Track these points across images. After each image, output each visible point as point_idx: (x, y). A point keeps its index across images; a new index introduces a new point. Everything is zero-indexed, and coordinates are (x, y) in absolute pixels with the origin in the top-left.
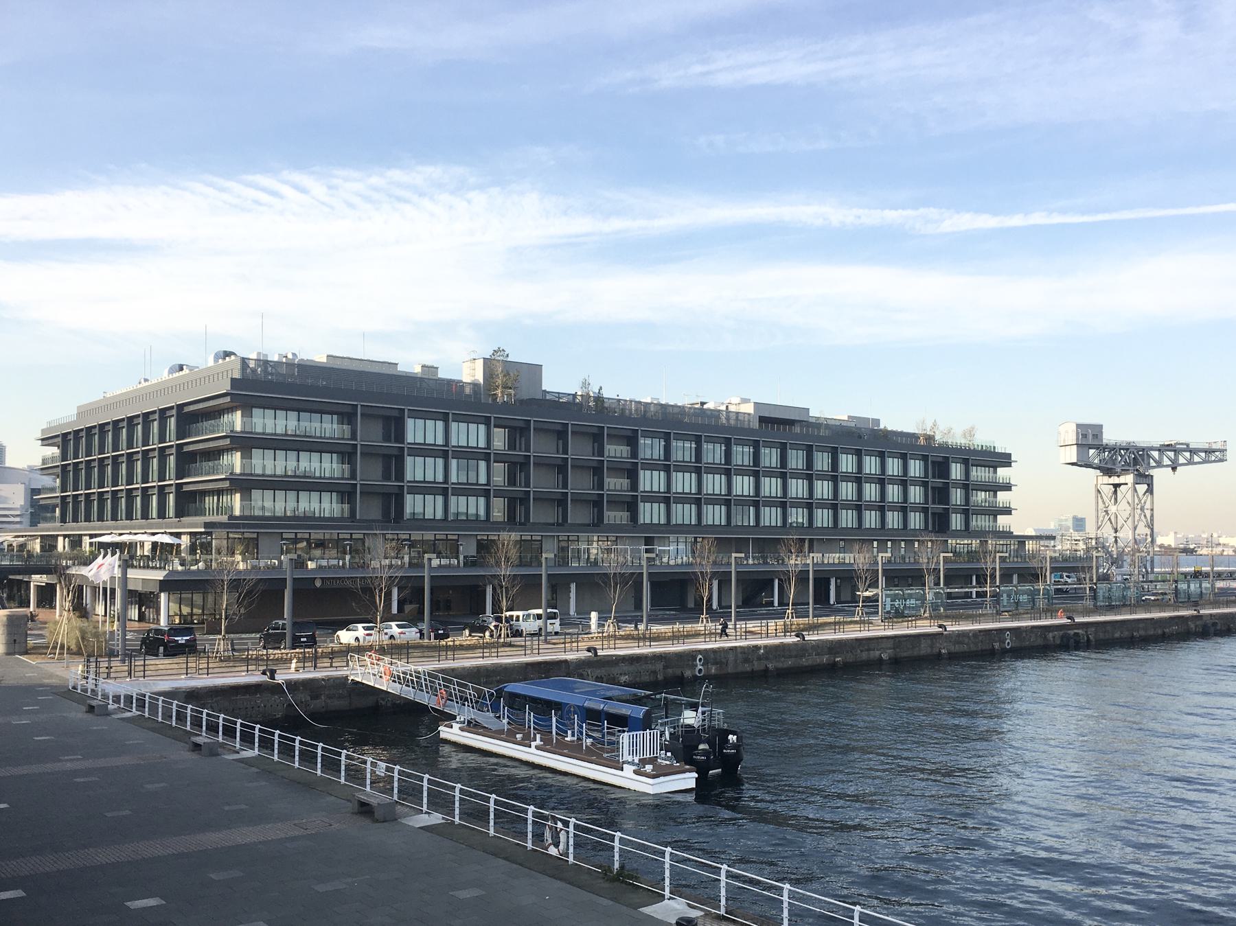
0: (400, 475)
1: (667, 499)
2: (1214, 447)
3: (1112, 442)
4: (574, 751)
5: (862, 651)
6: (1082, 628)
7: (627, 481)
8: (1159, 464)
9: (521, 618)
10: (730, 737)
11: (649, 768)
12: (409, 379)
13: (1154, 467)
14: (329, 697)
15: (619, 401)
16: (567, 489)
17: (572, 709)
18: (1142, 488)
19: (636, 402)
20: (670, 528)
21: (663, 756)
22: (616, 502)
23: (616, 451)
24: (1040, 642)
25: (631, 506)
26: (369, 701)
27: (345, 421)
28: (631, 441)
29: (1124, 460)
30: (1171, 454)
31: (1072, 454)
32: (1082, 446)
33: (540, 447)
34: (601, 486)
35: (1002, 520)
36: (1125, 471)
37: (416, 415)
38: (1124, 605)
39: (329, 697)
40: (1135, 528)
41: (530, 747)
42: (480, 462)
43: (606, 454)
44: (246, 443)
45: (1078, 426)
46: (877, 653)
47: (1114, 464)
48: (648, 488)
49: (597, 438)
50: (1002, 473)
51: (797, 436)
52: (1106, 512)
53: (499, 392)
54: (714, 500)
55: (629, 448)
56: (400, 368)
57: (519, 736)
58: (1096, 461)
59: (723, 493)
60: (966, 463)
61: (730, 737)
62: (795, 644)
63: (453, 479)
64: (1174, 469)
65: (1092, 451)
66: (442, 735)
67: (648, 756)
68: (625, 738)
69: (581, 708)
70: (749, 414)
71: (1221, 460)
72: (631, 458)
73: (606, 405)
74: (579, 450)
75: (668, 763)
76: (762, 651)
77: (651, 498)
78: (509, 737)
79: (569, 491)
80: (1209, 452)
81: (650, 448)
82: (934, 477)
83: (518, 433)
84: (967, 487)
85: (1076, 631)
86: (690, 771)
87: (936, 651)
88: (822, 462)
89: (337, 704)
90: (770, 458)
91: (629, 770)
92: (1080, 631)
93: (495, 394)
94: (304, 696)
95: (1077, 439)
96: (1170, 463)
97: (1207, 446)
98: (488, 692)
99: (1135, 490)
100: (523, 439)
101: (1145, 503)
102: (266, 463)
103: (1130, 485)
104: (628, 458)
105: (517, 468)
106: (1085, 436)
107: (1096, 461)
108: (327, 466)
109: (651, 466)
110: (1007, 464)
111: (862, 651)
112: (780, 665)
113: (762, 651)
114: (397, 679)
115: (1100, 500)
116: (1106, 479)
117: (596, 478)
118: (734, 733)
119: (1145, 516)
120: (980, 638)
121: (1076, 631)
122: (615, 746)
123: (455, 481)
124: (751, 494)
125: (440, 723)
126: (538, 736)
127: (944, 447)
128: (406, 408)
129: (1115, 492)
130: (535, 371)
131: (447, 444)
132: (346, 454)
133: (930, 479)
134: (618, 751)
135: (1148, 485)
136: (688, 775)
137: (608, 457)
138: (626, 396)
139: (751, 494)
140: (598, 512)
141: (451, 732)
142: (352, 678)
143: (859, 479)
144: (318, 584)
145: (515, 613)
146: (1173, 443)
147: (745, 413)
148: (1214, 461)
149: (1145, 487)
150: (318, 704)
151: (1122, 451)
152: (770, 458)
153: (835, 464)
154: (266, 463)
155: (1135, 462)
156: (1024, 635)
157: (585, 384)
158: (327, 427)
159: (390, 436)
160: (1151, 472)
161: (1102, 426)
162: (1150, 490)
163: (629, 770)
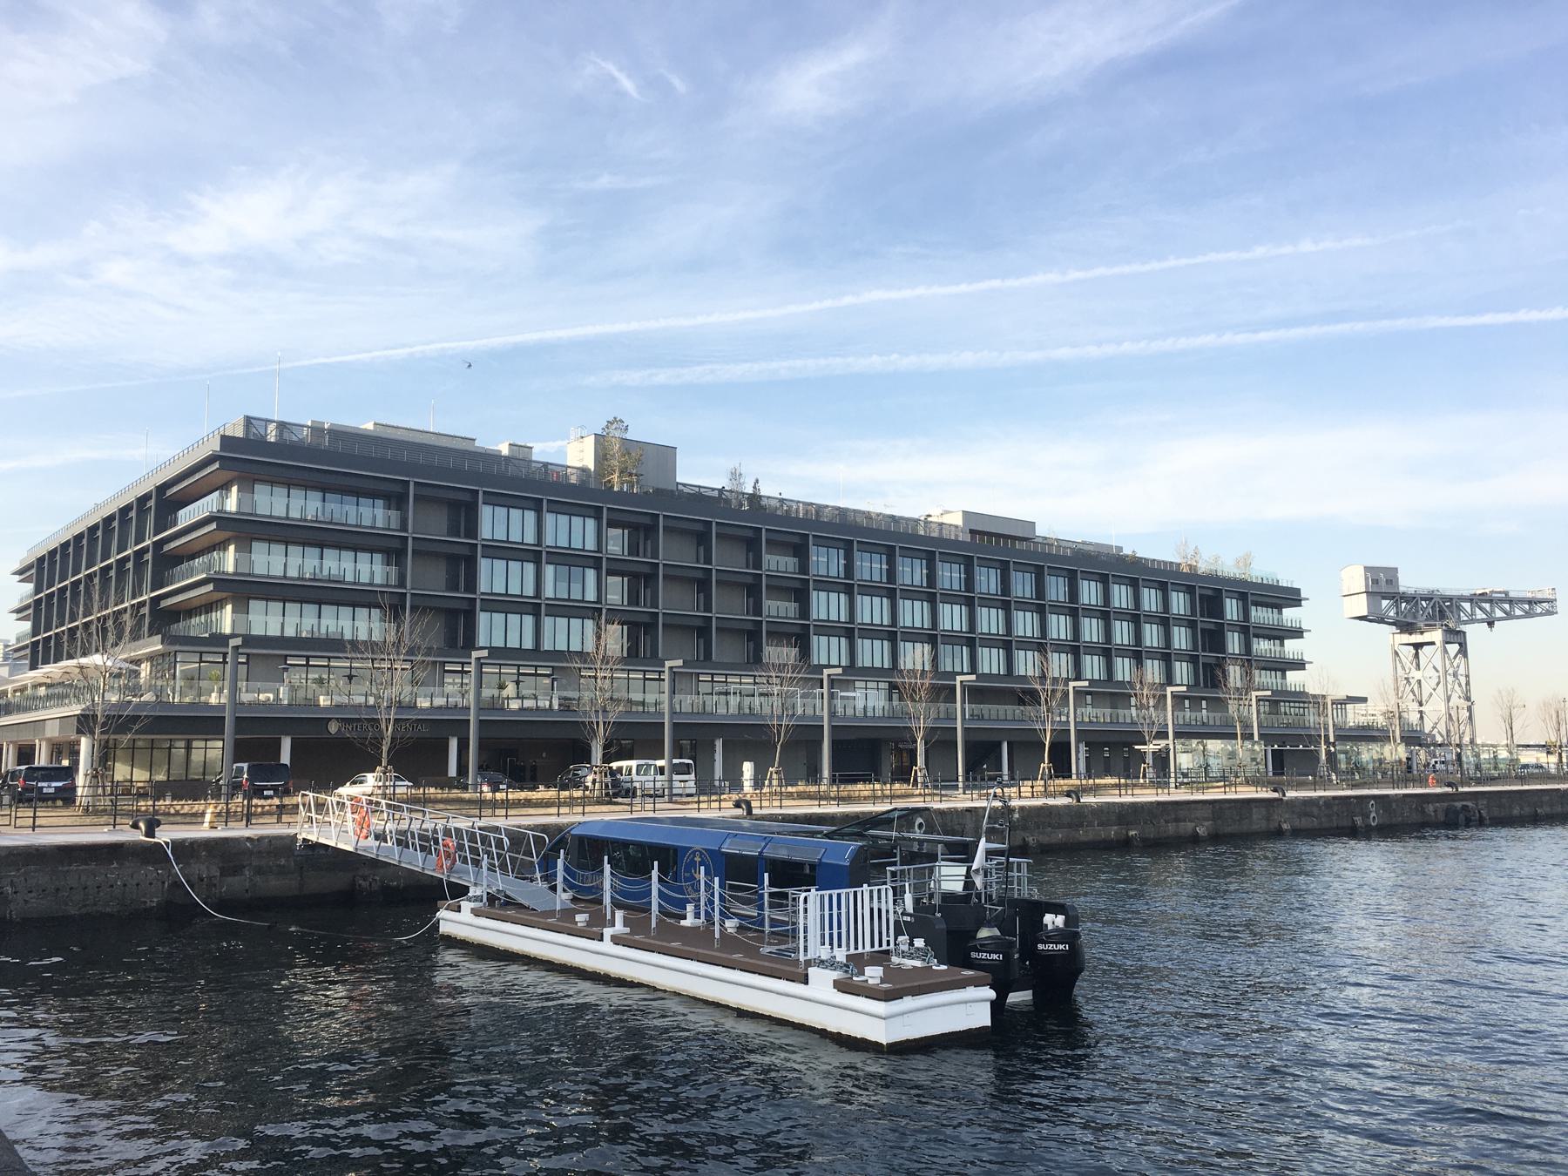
0: (472, 585)
1: (849, 632)
2: (1539, 596)
3: (1411, 591)
4: (697, 946)
5: (1167, 822)
6: (1470, 800)
7: (794, 652)
8: (1472, 621)
9: (634, 771)
10: (1048, 919)
11: (873, 974)
12: (492, 458)
13: (1465, 623)
14: (259, 871)
15: (782, 501)
16: (711, 612)
17: (698, 859)
18: (1453, 649)
19: (804, 503)
20: (854, 672)
21: (905, 948)
22: (781, 634)
23: (778, 563)
24: (1416, 818)
25: (801, 639)
26: (337, 881)
27: (393, 505)
28: (800, 550)
29: (1426, 614)
30: (1487, 606)
31: (1361, 606)
32: (1373, 594)
33: (671, 553)
34: (758, 610)
35: (1293, 678)
36: (1431, 627)
37: (496, 500)
38: (1493, 780)
39: (259, 871)
40: (1449, 699)
41: (601, 940)
42: (587, 570)
43: (765, 566)
44: (245, 530)
45: (1367, 569)
46: (1190, 826)
47: (1415, 617)
48: (823, 616)
49: (752, 544)
50: (1290, 615)
51: (1021, 553)
52: (1407, 679)
53: (615, 477)
54: (914, 636)
55: (796, 560)
56: (477, 444)
57: (581, 919)
58: (1392, 614)
59: (925, 627)
60: (1242, 597)
61: (1048, 919)
62: (1067, 807)
63: (549, 592)
64: (1491, 624)
65: (1385, 603)
66: (445, 928)
67: (868, 948)
68: (811, 904)
69: (716, 855)
70: (957, 527)
71: (1549, 613)
72: (800, 618)
73: (763, 503)
74: (726, 560)
75: (918, 963)
76: (1017, 816)
77: (828, 629)
78: (561, 923)
79: (714, 614)
80: (1530, 602)
81: (825, 562)
82: (1202, 616)
83: (642, 530)
84: (1248, 631)
85: (1465, 803)
86: (977, 983)
87: (1273, 825)
88: (1056, 589)
89: (274, 885)
90: (988, 581)
91: (822, 982)
92: (1469, 804)
93: (609, 481)
94: (201, 869)
95: (1367, 586)
96: (1484, 616)
97: (1530, 595)
98: (533, 836)
99: (1445, 651)
100: (649, 542)
101: (1458, 667)
102: (270, 561)
103: (1438, 644)
104: (795, 619)
105: (641, 579)
106: (1376, 582)
107: (1392, 614)
108: (368, 570)
109: (826, 585)
110: (1297, 603)
111: (1167, 822)
112: (1045, 839)
113: (1017, 816)
114: (402, 841)
115: (1399, 665)
116: (1406, 638)
117: (751, 600)
118: (1057, 909)
119: (1460, 685)
120: (1335, 809)
121: (1465, 803)
122: (787, 934)
123: (552, 596)
124: (964, 630)
125: (440, 903)
126: (619, 914)
127: (1213, 578)
128: (481, 490)
129: (1417, 656)
130: (666, 455)
131: (539, 544)
132: (391, 549)
133: (1198, 618)
134: (795, 937)
135: (1460, 644)
136: (971, 992)
137: (767, 617)
138: (791, 493)
139: (964, 630)
140: (754, 603)
141: (457, 921)
142: (304, 835)
143: (1105, 615)
144: (333, 728)
145: (624, 764)
146: (1487, 591)
147: (951, 525)
148: (1541, 614)
149: (1456, 647)
150: (236, 885)
151: (1423, 603)
152: (988, 581)
153: (1074, 594)
154: (270, 561)
155: (1443, 616)
156: (1394, 806)
157: (735, 475)
158: (372, 515)
159: (459, 532)
160: (1463, 628)
161: (1396, 569)
162: (1463, 651)
163: (822, 982)
